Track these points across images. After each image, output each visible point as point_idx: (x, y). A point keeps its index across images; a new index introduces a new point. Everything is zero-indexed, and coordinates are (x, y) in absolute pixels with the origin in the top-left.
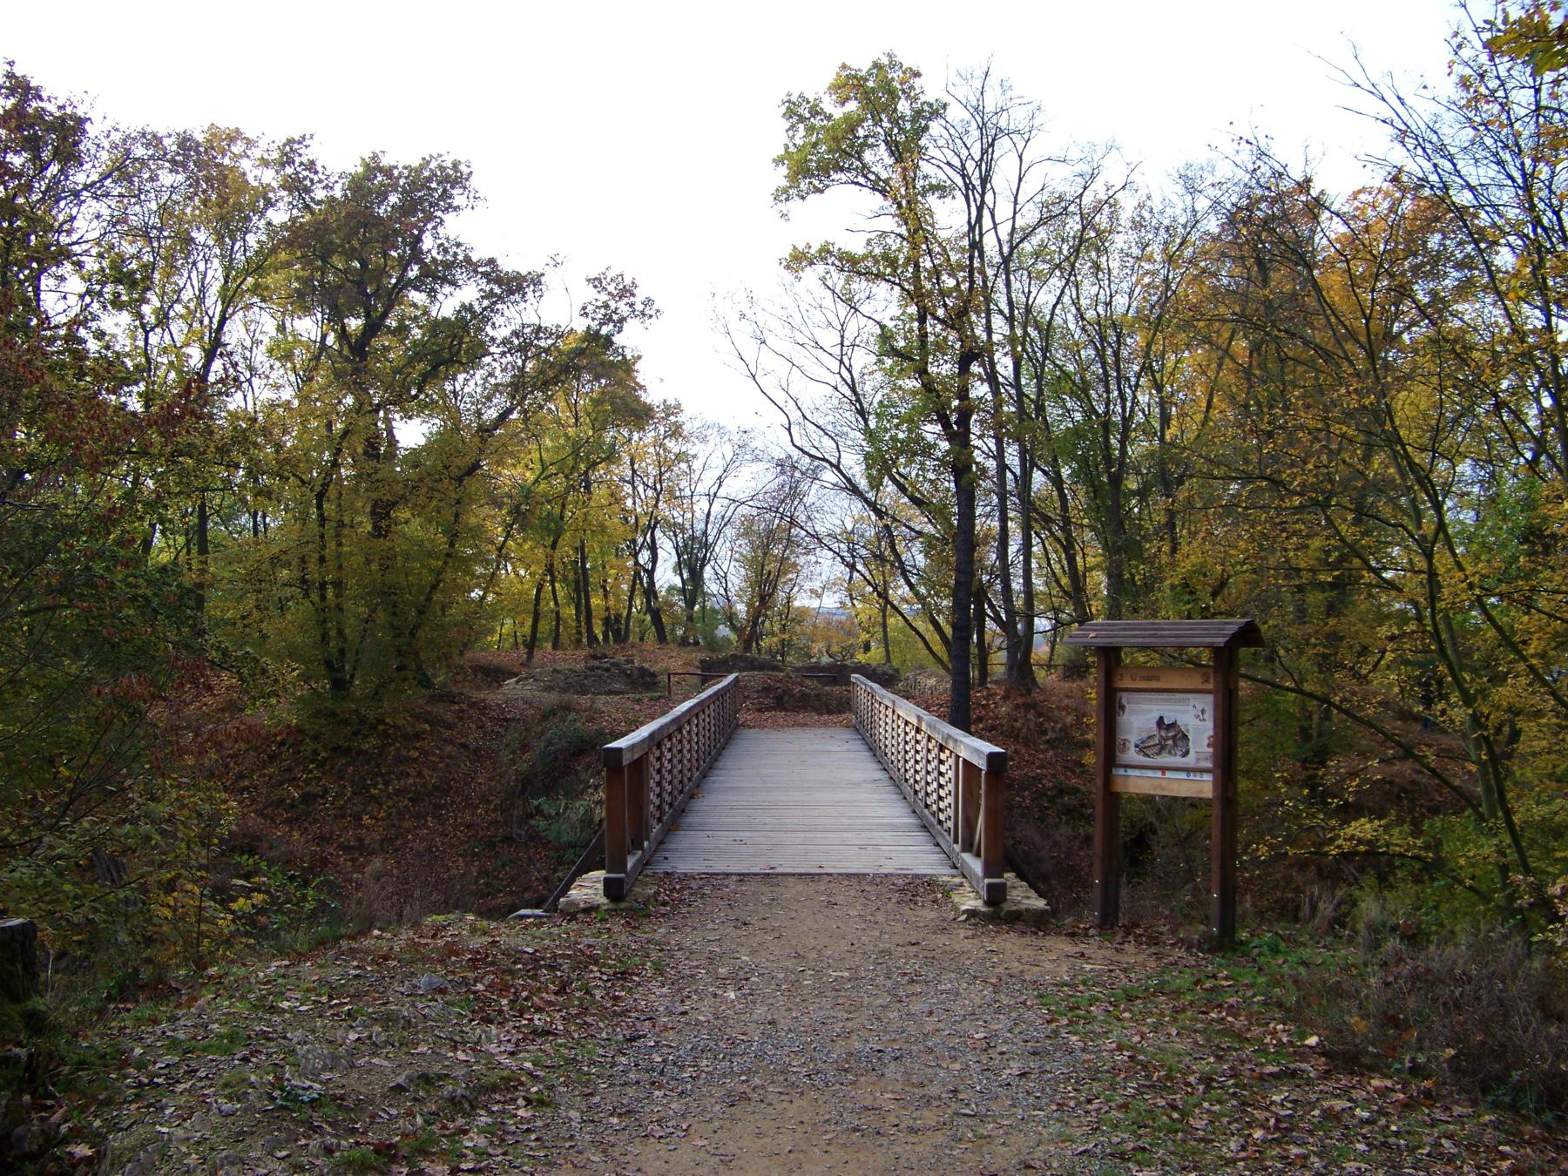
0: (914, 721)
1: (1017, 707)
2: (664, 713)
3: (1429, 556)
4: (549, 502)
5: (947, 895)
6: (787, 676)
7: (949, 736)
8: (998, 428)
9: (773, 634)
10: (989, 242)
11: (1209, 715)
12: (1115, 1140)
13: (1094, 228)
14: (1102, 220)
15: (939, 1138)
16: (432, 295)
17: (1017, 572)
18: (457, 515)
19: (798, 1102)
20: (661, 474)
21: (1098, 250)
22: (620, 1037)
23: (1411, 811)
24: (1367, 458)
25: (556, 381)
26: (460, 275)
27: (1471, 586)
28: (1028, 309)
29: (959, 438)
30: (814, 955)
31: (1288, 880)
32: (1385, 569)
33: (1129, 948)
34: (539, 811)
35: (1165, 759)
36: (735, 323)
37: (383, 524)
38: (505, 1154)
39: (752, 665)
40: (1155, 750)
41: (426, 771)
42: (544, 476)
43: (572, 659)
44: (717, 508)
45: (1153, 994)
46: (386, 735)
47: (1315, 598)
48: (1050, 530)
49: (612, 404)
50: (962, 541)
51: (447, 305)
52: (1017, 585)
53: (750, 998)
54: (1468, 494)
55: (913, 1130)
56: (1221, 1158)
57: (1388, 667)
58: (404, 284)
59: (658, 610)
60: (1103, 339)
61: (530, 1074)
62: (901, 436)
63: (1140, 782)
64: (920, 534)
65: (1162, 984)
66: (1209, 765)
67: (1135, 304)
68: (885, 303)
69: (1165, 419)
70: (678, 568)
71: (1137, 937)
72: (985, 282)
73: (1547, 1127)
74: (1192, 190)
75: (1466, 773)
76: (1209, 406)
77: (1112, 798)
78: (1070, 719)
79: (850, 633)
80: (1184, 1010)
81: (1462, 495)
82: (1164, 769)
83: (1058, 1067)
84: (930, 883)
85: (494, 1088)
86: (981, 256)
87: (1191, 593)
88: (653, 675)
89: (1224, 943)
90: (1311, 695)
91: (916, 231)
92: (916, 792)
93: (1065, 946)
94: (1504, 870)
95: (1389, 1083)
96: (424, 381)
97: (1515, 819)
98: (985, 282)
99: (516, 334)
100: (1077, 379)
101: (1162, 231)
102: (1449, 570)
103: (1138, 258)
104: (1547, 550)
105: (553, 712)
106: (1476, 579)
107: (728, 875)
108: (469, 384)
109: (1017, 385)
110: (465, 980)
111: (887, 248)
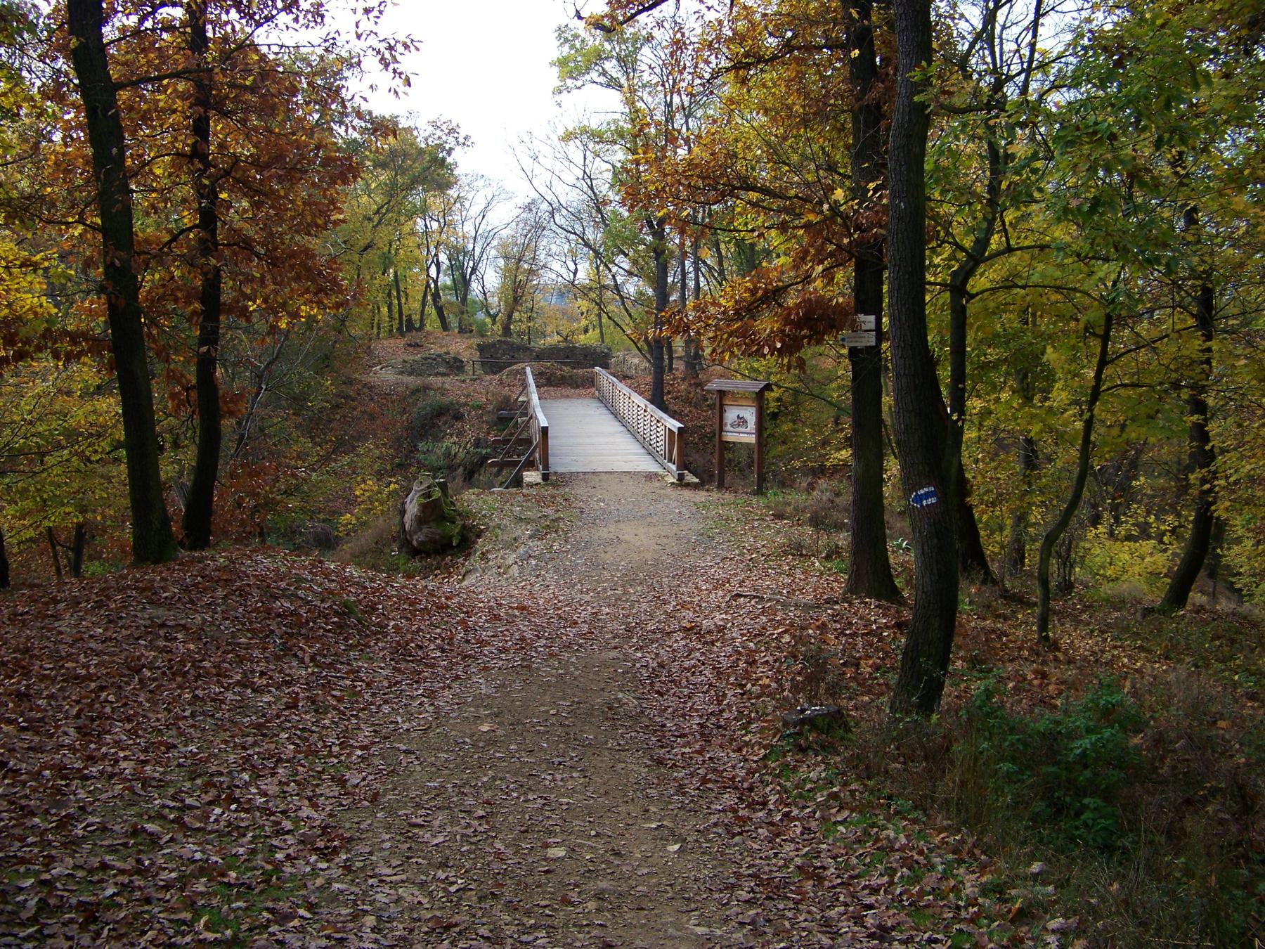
1: (691, 385)
35: (740, 429)
68: (619, 155)
84: (656, 474)
89: (760, 492)
93: (705, 493)
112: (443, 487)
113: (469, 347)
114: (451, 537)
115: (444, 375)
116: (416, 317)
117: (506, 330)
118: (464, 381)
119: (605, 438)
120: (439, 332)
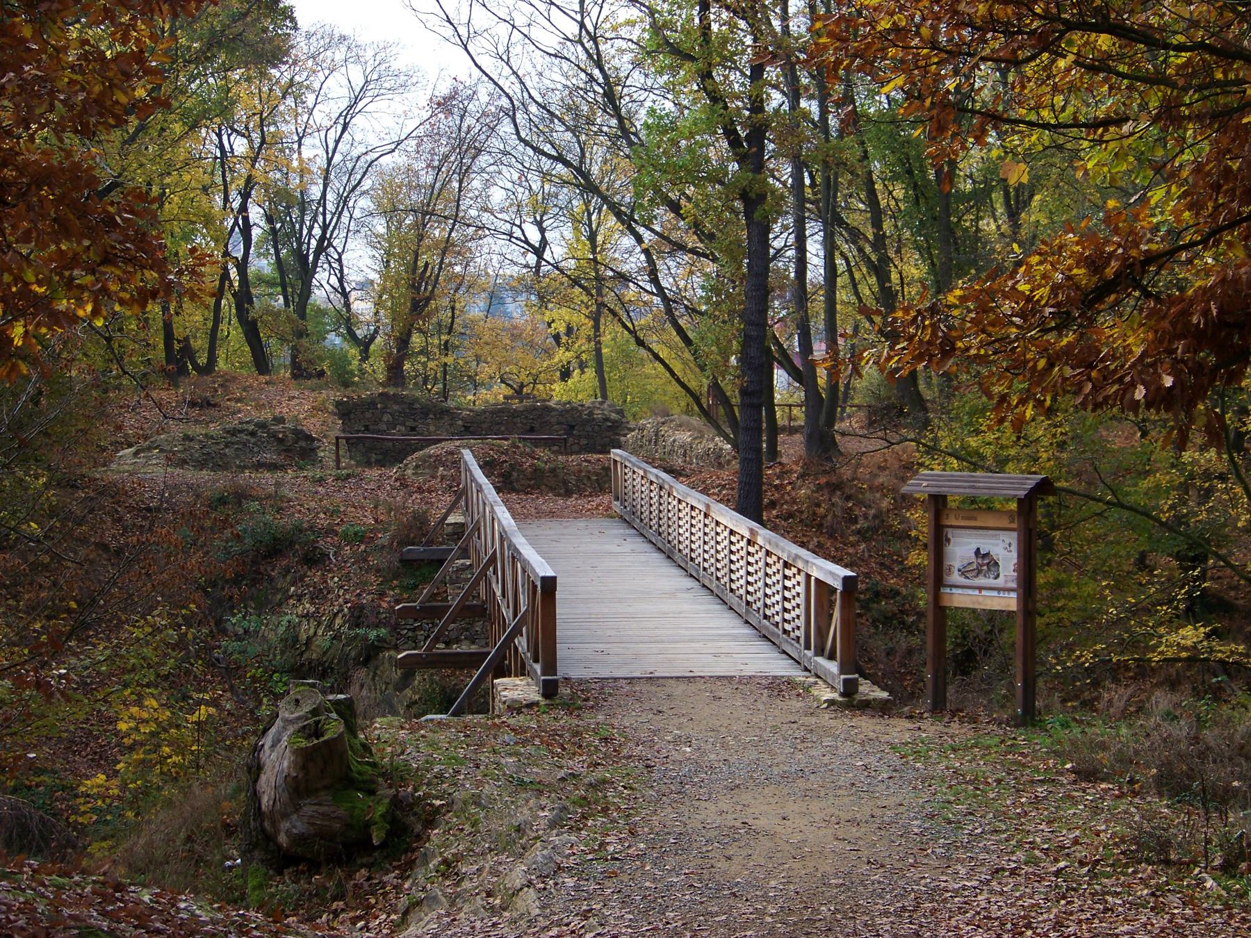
0: (747, 535)
1: (819, 488)
11: (1014, 548)
33: (955, 726)
35: (981, 581)
40: (974, 573)
59: (254, 322)
63: (963, 598)
66: (1014, 585)
77: (941, 611)
78: (885, 504)
82: (980, 589)
84: (790, 683)
89: (1029, 718)
93: (908, 724)
112: (347, 711)
113: (320, 408)
114: (367, 825)
115: (273, 467)
116: (200, 344)
117: (395, 372)
118: (321, 481)
119: (663, 602)
120: (247, 373)
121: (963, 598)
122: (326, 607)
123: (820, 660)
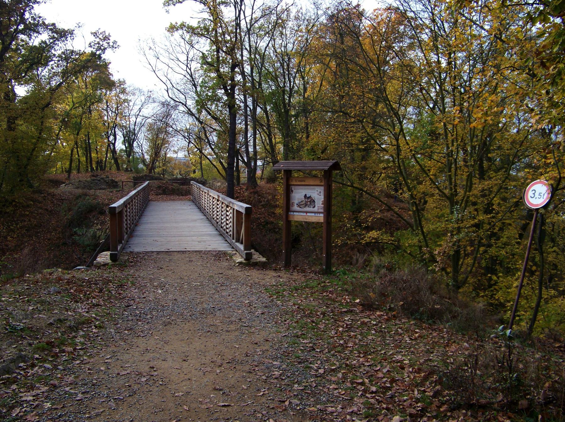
2: (126, 195)
3: (397, 140)
4: (76, 117)
5: (231, 257)
6: (167, 182)
7: (230, 202)
8: (245, 91)
9: (160, 167)
10: (243, 24)
11: (322, 194)
12: (294, 332)
13: (281, 19)
14: (284, 16)
15: (237, 333)
16: (30, 37)
17: (251, 143)
18: (42, 122)
19: (188, 324)
20: (118, 107)
21: (282, 27)
22: (124, 306)
23: (390, 229)
24: (377, 105)
25: (80, 72)
26: (41, 29)
27: (411, 150)
28: (256, 48)
29: (231, 95)
30: (186, 278)
31: (348, 254)
32: (382, 144)
33: (295, 274)
34: (76, 233)
35: (307, 209)
36: (147, 51)
37: (13, 126)
38: (91, 343)
39: (151, 178)
40: (304, 206)
41: (32, 220)
42: (74, 107)
43: (85, 177)
44: (139, 119)
45: (304, 288)
46: (16, 206)
47: (358, 154)
48: (263, 129)
49: (100, 81)
50: (230, 133)
51: (36, 40)
52: (251, 149)
53: (167, 292)
54: (411, 118)
55: (227, 331)
56: (329, 336)
57: (383, 179)
58: (17, 31)
60: (283, 60)
61: (95, 318)
62: (210, 94)
63: (299, 217)
64: (215, 130)
65: (307, 285)
66: (322, 211)
67: (295, 47)
68: (204, 45)
69: (305, 89)
70: (124, 143)
71: (297, 270)
72: (241, 38)
73: (430, 324)
74: (318, 8)
75: (409, 216)
76: (321, 85)
77: (288, 222)
78: (270, 197)
79: (188, 167)
80: (315, 293)
81: (409, 119)
82: (307, 212)
83: (274, 311)
84: (225, 253)
85: (84, 323)
86: (240, 28)
87: (314, 152)
88: (116, 182)
89: (327, 271)
90: (356, 188)
91: (216, 19)
92: (217, 223)
94: (420, 247)
95: (382, 313)
96: (28, 71)
97: (424, 230)
98: (241, 38)
99: (63, 53)
100: (274, 74)
101: (305, 21)
102: (404, 145)
103: (297, 31)
104: (437, 139)
105: (80, 196)
106: (413, 148)
107: (153, 252)
108: (44, 72)
109: (252, 76)
110: (67, 289)
111: (205, 24)
121: (299, 217)
122: (104, 227)
123: (238, 244)
